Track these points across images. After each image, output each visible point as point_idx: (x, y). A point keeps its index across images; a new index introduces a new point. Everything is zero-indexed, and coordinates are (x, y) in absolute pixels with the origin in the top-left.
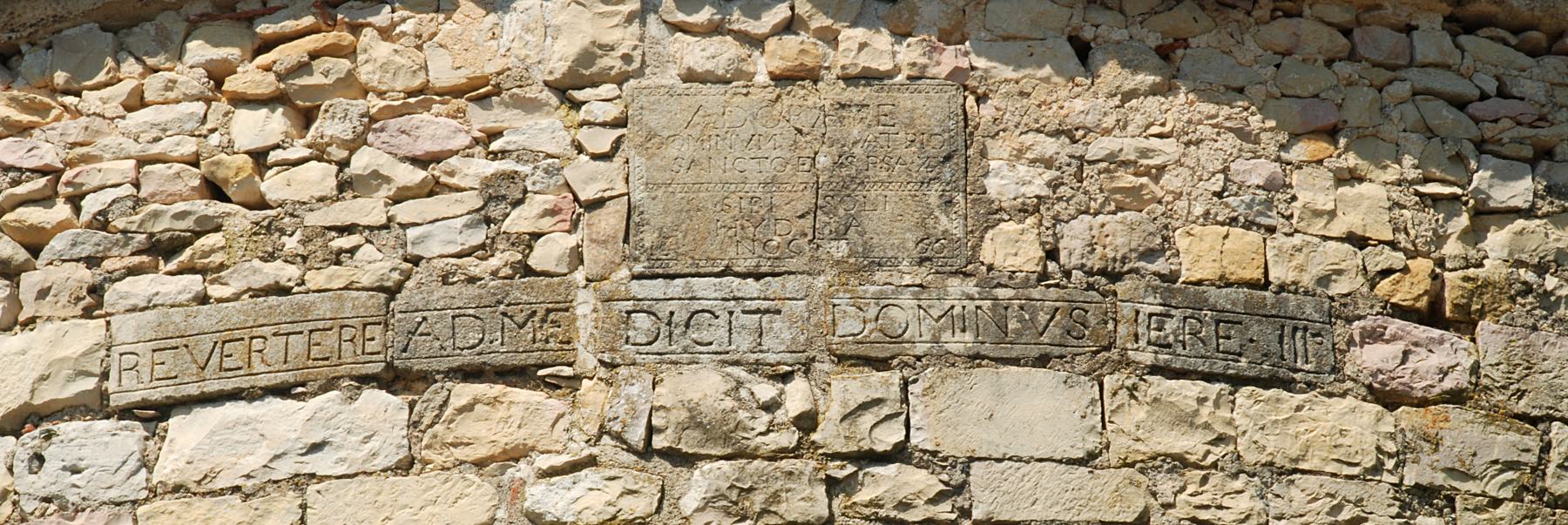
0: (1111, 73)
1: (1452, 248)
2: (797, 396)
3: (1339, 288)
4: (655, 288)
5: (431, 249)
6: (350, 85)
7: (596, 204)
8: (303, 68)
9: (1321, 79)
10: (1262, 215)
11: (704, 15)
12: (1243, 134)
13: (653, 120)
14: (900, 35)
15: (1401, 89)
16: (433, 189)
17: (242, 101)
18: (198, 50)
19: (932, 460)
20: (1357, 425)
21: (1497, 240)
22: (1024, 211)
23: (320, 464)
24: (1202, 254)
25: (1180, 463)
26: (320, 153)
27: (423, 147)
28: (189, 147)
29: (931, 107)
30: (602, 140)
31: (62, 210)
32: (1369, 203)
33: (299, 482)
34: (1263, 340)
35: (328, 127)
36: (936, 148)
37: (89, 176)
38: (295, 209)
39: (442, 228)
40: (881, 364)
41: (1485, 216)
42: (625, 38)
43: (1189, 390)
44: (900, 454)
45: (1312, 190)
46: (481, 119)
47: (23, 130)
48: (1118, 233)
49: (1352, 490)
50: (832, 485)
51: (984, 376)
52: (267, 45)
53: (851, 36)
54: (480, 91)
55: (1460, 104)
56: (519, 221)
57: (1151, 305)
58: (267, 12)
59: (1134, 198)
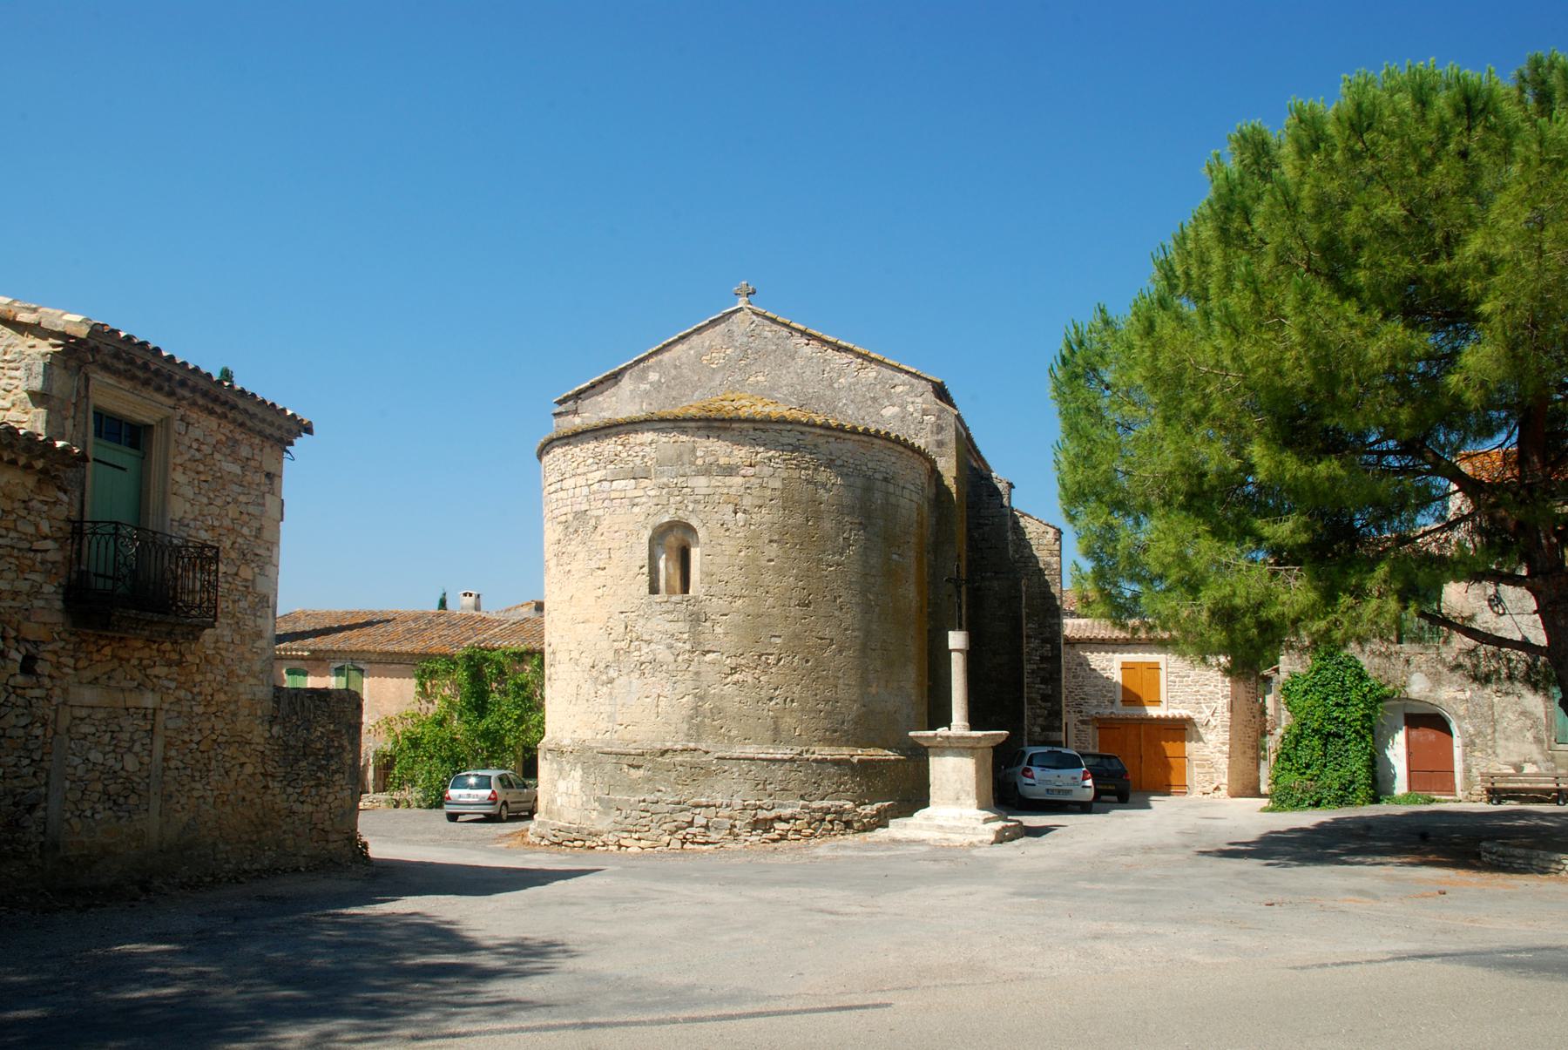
20: (740, 480)
24: (722, 461)
34: (730, 471)
39: (638, 461)
48: (712, 459)
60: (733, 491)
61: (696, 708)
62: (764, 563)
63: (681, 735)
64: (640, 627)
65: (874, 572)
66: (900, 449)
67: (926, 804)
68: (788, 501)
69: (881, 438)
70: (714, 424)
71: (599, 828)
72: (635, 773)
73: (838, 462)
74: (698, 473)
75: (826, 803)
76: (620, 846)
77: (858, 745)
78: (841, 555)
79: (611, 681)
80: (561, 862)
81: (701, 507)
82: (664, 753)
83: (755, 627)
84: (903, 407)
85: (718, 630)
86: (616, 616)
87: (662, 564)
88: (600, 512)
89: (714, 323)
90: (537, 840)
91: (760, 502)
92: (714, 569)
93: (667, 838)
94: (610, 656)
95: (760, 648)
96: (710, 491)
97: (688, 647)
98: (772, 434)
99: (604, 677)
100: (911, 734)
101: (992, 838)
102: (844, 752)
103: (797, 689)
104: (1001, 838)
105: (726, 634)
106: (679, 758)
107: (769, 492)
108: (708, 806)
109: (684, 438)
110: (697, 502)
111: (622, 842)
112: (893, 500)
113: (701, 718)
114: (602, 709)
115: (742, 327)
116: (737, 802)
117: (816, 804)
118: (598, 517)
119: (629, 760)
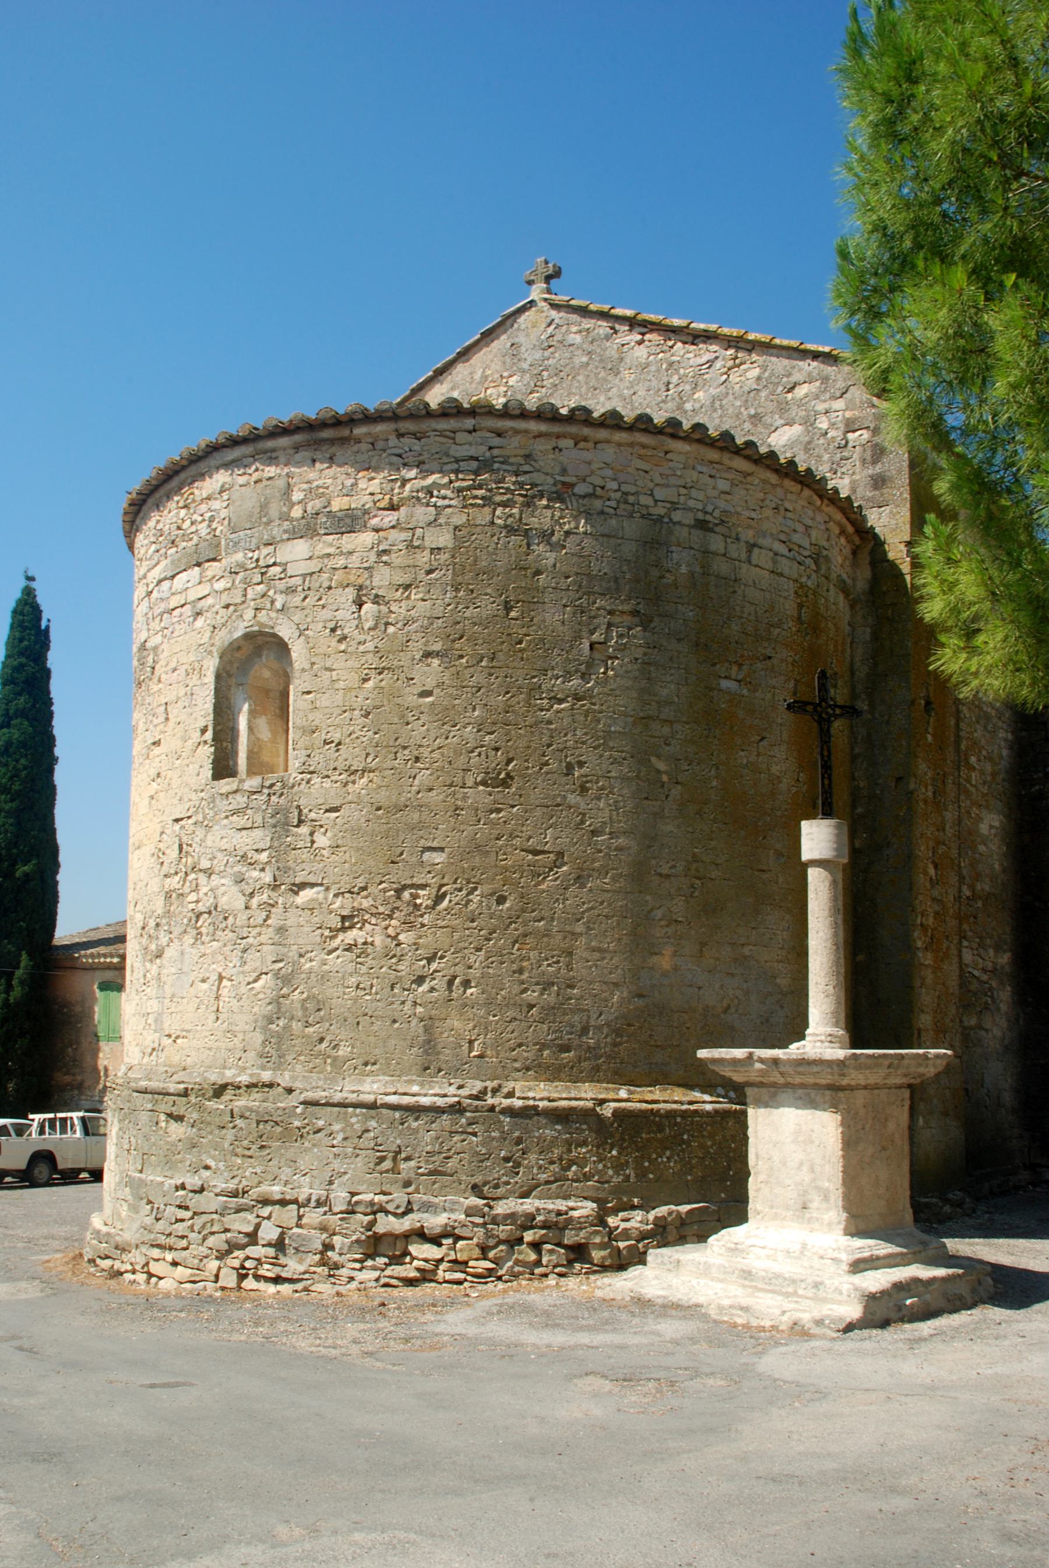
1: (396, 491)
2: (256, 555)
3: (367, 507)
21: (408, 487)
22: (299, 503)
23: (189, 585)
34: (350, 522)
40: (271, 544)
41: (404, 482)
42: (228, 479)
44: (274, 564)
49: (366, 554)
51: (290, 542)
61: (277, 1001)
63: (251, 1055)
65: (667, 713)
66: (740, 463)
67: (741, 1217)
68: (464, 571)
69: (687, 438)
70: (323, 435)
72: (177, 1131)
73: (581, 489)
74: (295, 535)
75: (529, 1205)
77: (621, 1078)
78: (585, 676)
80: (972, 1244)
81: (297, 600)
82: (219, 1091)
84: (809, 422)
85: (322, 840)
89: (489, 336)
91: (406, 579)
95: (400, 875)
96: (314, 566)
97: (267, 878)
98: (434, 442)
100: (702, 1054)
101: (854, 1311)
103: (477, 959)
104: (883, 1312)
106: (240, 1103)
108: (283, 1203)
109: (271, 471)
111: (154, 1267)
112: (721, 567)
113: (290, 1021)
115: (534, 334)
116: (340, 1197)
117: (501, 1208)
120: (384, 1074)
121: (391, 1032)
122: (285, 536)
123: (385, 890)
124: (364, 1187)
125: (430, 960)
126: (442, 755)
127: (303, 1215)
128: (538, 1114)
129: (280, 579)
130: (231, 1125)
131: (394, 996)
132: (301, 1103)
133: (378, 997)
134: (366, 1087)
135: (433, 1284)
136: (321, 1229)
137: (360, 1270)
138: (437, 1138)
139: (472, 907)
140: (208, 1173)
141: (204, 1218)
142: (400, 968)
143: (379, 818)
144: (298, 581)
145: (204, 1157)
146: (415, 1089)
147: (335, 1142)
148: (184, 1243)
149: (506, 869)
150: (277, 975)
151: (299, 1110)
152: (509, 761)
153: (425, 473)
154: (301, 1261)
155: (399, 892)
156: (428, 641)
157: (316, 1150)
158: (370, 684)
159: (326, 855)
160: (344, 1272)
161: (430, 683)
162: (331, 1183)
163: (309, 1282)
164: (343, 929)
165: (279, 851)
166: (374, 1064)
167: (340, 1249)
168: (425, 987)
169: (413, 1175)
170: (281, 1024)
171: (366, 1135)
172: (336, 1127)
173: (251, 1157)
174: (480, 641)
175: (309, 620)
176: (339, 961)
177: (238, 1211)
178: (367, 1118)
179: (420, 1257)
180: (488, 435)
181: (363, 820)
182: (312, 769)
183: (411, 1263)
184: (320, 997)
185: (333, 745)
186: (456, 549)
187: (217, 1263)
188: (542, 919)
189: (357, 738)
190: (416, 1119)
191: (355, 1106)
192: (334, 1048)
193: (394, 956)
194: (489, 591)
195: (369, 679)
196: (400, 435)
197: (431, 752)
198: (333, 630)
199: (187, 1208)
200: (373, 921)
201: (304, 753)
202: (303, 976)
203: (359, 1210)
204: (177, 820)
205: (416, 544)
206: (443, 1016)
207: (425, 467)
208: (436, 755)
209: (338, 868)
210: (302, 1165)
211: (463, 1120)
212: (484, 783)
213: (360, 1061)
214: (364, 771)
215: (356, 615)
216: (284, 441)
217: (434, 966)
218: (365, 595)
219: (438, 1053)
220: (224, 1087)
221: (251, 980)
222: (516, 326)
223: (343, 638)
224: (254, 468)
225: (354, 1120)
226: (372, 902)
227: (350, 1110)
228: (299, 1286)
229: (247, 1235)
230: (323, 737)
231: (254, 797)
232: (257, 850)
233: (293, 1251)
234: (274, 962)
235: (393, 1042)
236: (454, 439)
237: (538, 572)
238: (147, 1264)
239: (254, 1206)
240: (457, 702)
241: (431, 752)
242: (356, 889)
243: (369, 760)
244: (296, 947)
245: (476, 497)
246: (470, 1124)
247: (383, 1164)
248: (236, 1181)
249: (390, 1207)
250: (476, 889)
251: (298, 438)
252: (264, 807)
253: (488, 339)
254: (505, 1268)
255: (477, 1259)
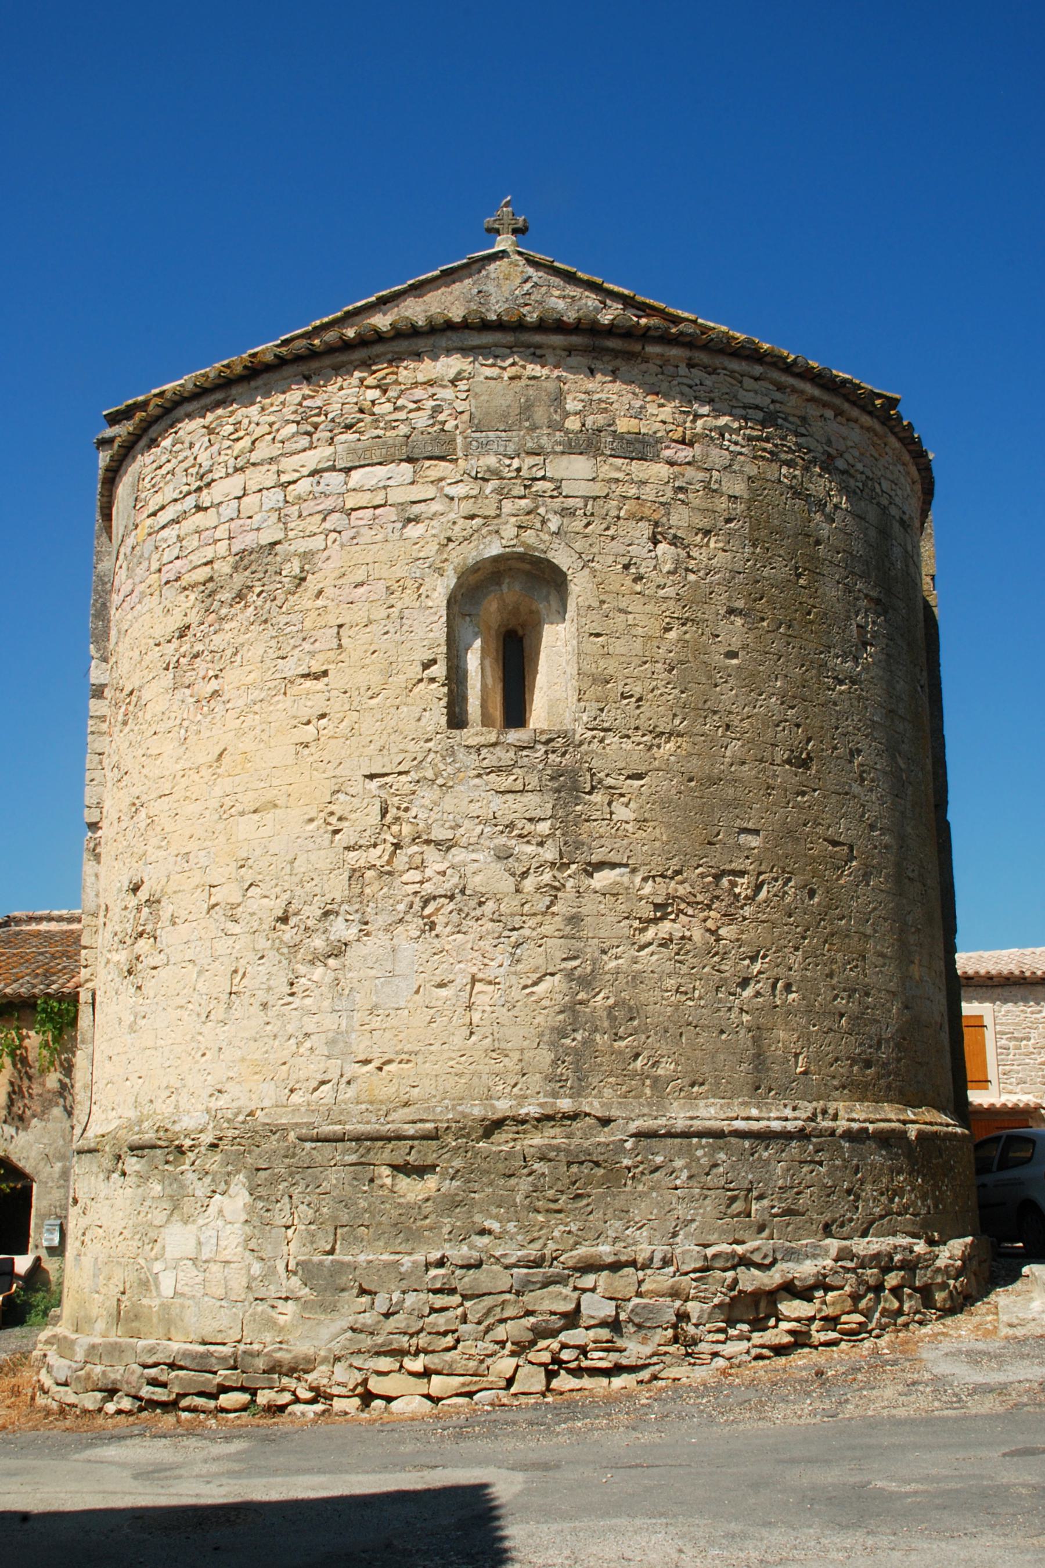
0: (599, 377)
1: (688, 425)
2: (516, 463)
3: (659, 435)
4: (478, 435)
5: (418, 426)
6: (397, 382)
7: (462, 413)
8: (384, 378)
9: (653, 379)
10: (639, 415)
11: (491, 361)
12: (634, 393)
13: (477, 390)
14: (543, 367)
15: (675, 382)
16: (419, 409)
17: (368, 387)
18: (357, 374)
19: (551, 480)
20: (662, 470)
21: (700, 423)
22: (576, 414)
23: (390, 483)
24: (623, 425)
25: (617, 480)
26: (389, 401)
27: (416, 398)
28: (355, 400)
29: (551, 386)
30: (464, 395)
31: (323, 418)
32: (667, 412)
33: (385, 487)
34: (639, 448)
35: (391, 394)
36: (553, 397)
37: (329, 408)
38: (382, 416)
39: (421, 419)
40: (538, 454)
41: (697, 416)
42: (469, 368)
43: (620, 461)
44: (543, 478)
45: (652, 409)
46: (431, 390)
47: (313, 397)
48: (601, 419)
49: (662, 488)
50: (526, 487)
51: (565, 457)
52: (375, 372)
53: (530, 367)
54: (430, 383)
55: (690, 387)
56: (441, 417)
57: (610, 439)
58: (375, 364)
59: (605, 410)
60: (648, 493)
61: (572, 1008)
62: (718, 659)
63: (535, 1080)
64: (426, 809)
68: (760, 530)
71: (301, 1347)
72: (413, 1190)
74: (571, 448)
76: (368, 1398)
79: (339, 950)
81: (578, 525)
82: (493, 1127)
83: (704, 803)
86: (358, 786)
87: (473, 661)
88: (318, 543)
90: (90, 1401)
91: (704, 523)
92: (611, 666)
93: (505, 1365)
94: (337, 887)
95: (716, 859)
96: (598, 489)
99: (318, 943)
102: (889, 1115)
103: (795, 959)
105: (642, 822)
107: (722, 504)
108: (615, 1267)
109: (534, 369)
110: (566, 512)
111: (375, 1385)
113: (586, 1033)
114: (310, 1026)
115: (507, 287)
116: (688, 1250)
118: (307, 556)
119: (399, 1153)
120: (714, 1097)
121: (719, 1045)
122: (559, 448)
123: (702, 876)
124: (715, 1236)
125: (753, 959)
126: (752, 724)
127: (643, 1280)
128: (869, 1138)
129: (552, 497)
130: (525, 1171)
131: (720, 1001)
132: (631, 1136)
133: (702, 1003)
134: (702, 1112)
135: (807, 1350)
136: (671, 1295)
137: (724, 1342)
138: (788, 1170)
139: (788, 899)
140: (486, 1240)
141: (488, 1301)
142: (723, 967)
143: (692, 790)
144: (579, 503)
145: (478, 1218)
146: (754, 1112)
147: (678, 1182)
148: (449, 1340)
149: (814, 859)
150: (570, 975)
151: (628, 1145)
152: (809, 740)
153: (718, 413)
154: (644, 1341)
155: (717, 877)
156: (730, 597)
157: (654, 1194)
158: (672, 635)
159: (631, 830)
160: (703, 1347)
161: (736, 644)
162: (675, 1235)
163: (657, 1367)
164: (656, 921)
165: (568, 824)
166: (702, 1084)
167: (699, 1318)
168: (749, 992)
169: (767, 1217)
170: (579, 1038)
171: (714, 1171)
172: (679, 1163)
173: (559, 1211)
174: (778, 606)
175: (595, 550)
176: (650, 959)
177: (545, 1285)
178: (715, 1149)
179: (572, 1343)
180: (771, 387)
181: (674, 791)
182: (606, 725)
183: (776, 1326)
184: (632, 1003)
185: (633, 700)
186: (751, 500)
187: (513, 1361)
188: (843, 917)
189: (661, 695)
190: (766, 1148)
191: (700, 1135)
192: (653, 1066)
193: (717, 953)
194: (782, 552)
195: (671, 629)
196: (691, 366)
197: (742, 720)
198: (626, 567)
199: (452, 1291)
200: (690, 912)
201: (596, 705)
202: (608, 977)
203: (717, 1265)
204: (371, 777)
205: (715, 487)
206: (770, 1025)
207: (717, 406)
208: (745, 724)
209: (649, 844)
210: (636, 1214)
211: (811, 1147)
212: (788, 762)
213: (687, 1081)
214: (671, 734)
215: (653, 554)
216: (557, 340)
217: (757, 967)
218: (660, 533)
219: (768, 1069)
220: (498, 1124)
221: (530, 982)
222: (484, 273)
223: (638, 578)
224: (510, 361)
225: (699, 1153)
226: (689, 889)
227: (695, 1140)
228: (645, 1375)
229: (564, 1315)
230: (620, 689)
231: (524, 753)
232: (530, 820)
233: (633, 1330)
234: (564, 959)
235: (722, 1057)
236: (741, 382)
237: (818, 543)
238: (365, 1382)
239: (569, 1276)
240: (761, 668)
241: (742, 720)
242: (670, 872)
243: (677, 722)
244: (596, 941)
245: (764, 450)
246: (817, 1151)
247: (734, 1206)
248: (538, 1245)
249: (757, 1258)
250: (789, 880)
251: (575, 340)
252: (541, 767)
253: (448, 279)
254: (875, 1321)
255: (848, 1313)
